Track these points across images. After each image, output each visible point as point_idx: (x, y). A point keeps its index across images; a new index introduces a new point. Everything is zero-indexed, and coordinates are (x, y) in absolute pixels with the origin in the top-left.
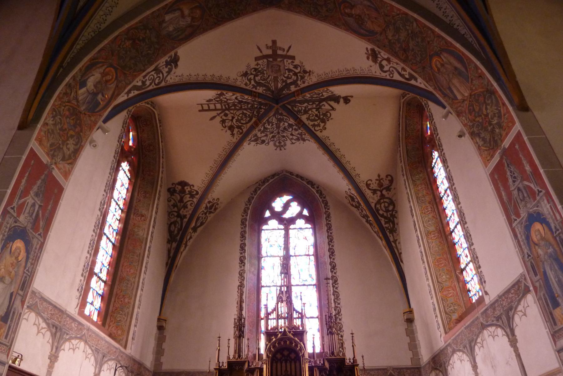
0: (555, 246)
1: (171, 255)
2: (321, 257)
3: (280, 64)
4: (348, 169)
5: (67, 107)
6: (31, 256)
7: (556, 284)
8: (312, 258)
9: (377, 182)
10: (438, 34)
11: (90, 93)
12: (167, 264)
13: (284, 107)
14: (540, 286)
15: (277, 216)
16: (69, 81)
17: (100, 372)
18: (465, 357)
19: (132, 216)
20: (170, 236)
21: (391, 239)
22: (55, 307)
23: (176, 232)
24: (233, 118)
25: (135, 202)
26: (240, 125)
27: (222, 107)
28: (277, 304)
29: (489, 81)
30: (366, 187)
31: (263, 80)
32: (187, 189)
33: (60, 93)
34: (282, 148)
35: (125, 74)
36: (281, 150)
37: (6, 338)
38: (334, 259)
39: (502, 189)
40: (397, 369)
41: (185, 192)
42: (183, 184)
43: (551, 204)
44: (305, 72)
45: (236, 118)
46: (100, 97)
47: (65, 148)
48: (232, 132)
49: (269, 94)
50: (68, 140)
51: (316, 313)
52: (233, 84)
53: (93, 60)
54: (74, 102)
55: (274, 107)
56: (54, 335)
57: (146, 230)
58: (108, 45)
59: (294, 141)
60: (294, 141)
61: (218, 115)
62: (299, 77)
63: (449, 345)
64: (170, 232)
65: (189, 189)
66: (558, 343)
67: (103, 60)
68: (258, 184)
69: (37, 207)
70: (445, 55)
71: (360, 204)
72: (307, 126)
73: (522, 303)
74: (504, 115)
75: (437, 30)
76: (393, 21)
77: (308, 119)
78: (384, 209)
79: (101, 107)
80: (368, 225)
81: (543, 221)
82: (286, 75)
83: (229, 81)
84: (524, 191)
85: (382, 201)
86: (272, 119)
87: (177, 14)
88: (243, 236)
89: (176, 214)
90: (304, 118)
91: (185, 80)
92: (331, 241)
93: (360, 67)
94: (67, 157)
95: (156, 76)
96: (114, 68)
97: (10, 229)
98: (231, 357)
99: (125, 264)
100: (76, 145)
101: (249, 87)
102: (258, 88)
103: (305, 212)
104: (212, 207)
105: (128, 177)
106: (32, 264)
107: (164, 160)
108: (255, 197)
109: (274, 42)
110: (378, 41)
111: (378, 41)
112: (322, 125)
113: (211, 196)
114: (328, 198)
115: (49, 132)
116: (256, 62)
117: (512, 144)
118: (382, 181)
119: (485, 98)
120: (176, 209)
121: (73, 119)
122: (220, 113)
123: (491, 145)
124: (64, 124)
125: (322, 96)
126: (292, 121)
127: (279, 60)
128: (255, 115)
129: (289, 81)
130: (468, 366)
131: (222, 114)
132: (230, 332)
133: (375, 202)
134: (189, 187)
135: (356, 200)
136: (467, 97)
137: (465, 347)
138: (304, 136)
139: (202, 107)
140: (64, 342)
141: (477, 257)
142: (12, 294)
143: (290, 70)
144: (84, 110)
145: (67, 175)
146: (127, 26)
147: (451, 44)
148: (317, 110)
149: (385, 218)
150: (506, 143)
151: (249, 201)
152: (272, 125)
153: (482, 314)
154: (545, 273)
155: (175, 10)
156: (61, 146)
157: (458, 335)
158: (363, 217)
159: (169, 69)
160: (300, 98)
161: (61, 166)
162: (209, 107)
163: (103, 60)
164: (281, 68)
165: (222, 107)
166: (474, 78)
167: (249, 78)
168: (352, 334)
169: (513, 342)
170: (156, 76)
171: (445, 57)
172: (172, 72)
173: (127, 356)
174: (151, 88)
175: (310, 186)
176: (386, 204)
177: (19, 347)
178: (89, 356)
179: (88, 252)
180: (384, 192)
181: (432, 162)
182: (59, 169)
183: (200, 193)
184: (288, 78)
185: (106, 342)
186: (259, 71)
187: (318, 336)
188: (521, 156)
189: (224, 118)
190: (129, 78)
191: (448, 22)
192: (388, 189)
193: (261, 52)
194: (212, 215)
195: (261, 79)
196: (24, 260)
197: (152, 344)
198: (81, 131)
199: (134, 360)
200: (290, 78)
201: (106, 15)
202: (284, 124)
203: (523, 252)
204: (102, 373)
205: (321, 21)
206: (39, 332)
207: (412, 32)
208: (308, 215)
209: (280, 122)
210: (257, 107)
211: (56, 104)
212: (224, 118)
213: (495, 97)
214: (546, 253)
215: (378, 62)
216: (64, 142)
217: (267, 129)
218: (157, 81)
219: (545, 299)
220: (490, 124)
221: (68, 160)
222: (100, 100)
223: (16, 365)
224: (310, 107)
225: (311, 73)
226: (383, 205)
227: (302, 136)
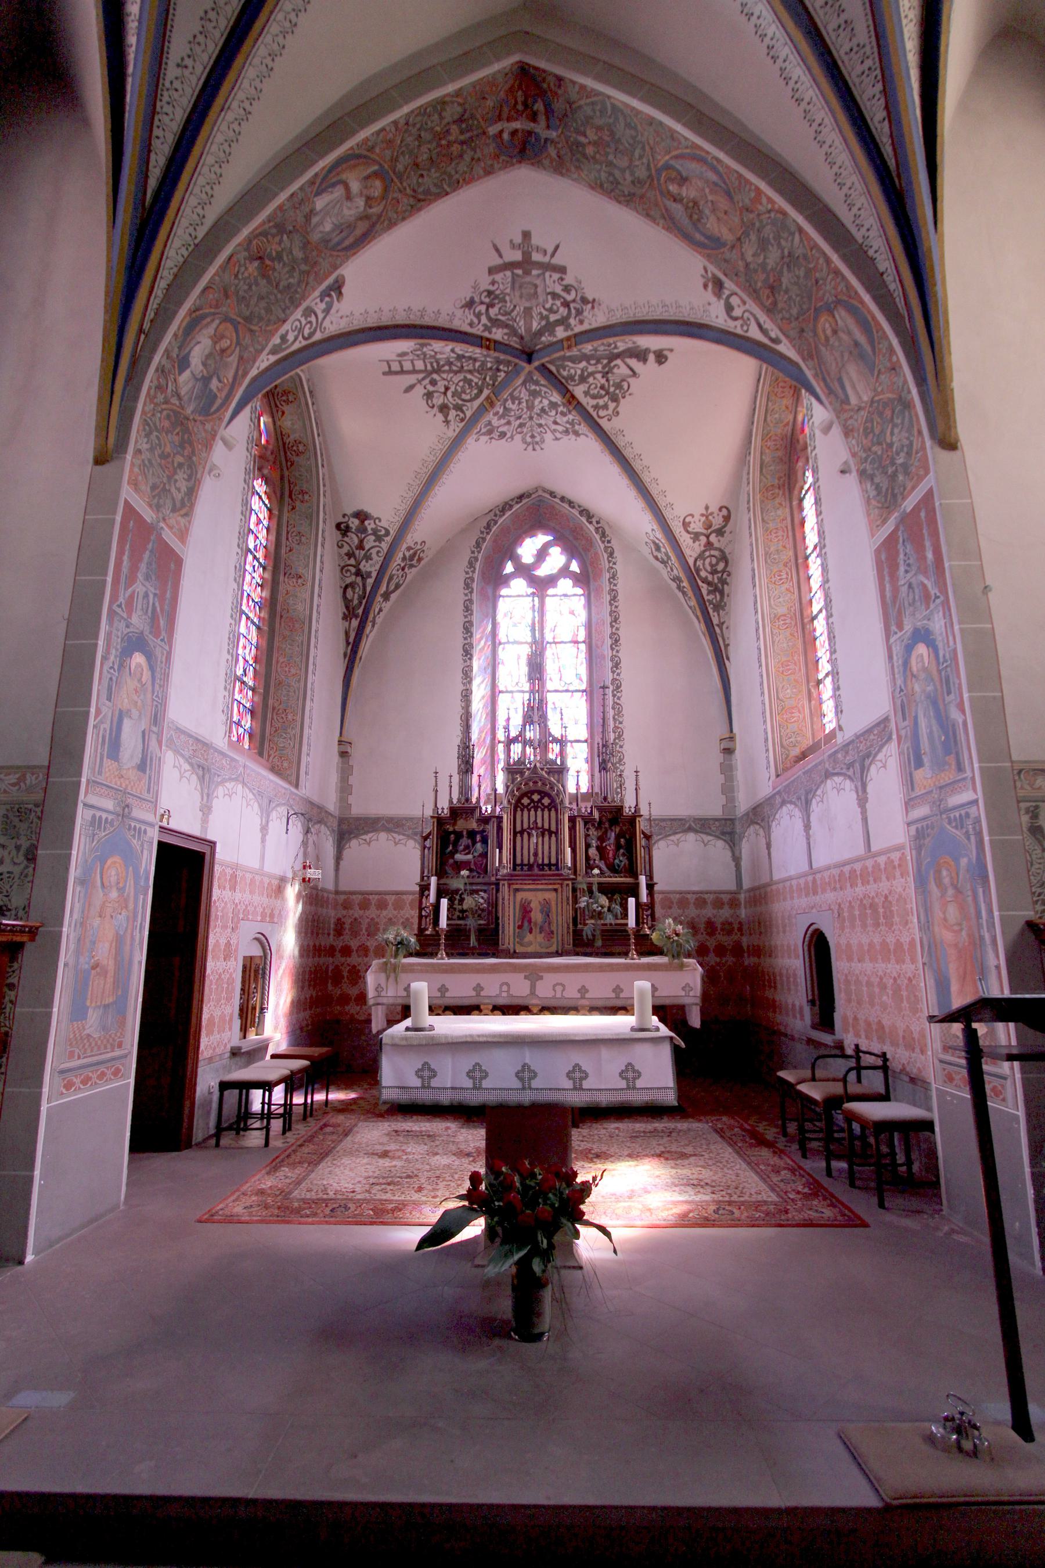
0: (938, 683)
1: (351, 640)
2: (597, 647)
3: (538, 282)
4: (654, 492)
5: (165, 413)
6: (158, 675)
7: (925, 736)
8: (583, 647)
9: (703, 519)
10: (836, 267)
11: (197, 380)
12: (345, 655)
13: (543, 369)
14: (906, 736)
15: (524, 571)
16: (160, 362)
17: (267, 822)
18: (797, 813)
19: (282, 578)
20: (347, 607)
21: (715, 621)
22: (197, 740)
23: (356, 602)
24: (447, 389)
25: (283, 551)
26: (460, 402)
27: (426, 366)
28: (524, 726)
29: (905, 382)
30: (682, 529)
31: (503, 315)
32: (369, 525)
33: (150, 388)
34: (537, 447)
35: (251, 331)
36: (534, 449)
37: (149, 791)
38: (618, 651)
39: (887, 578)
40: (701, 820)
41: (365, 530)
42: (362, 516)
43: (947, 620)
44: (584, 301)
45: (453, 389)
46: (214, 384)
47: (173, 490)
48: (446, 416)
49: (514, 342)
50: (175, 473)
51: (584, 734)
52: (447, 325)
53: (197, 310)
54: (175, 401)
55: (523, 368)
56: (202, 779)
57: (308, 601)
58: (217, 278)
59: (558, 435)
60: (558, 435)
61: (420, 382)
62: (573, 311)
63: (779, 793)
64: (347, 602)
65: (373, 526)
66: (910, 814)
67: (212, 310)
68: (492, 514)
69: (151, 596)
70: (843, 313)
71: (669, 558)
72: (585, 409)
73: (884, 750)
74: (917, 453)
75: (835, 257)
76: (757, 224)
77: (586, 393)
78: (709, 569)
79: (219, 402)
80: (680, 595)
81: (931, 644)
82: (548, 306)
83: (440, 320)
84: (917, 591)
85: (707, 554)
86: (520, 392)
87: (339, 192)
88: (468, 609)
89: (353, 570)
90: (579, 391)
91: (358, 323)
92: (615, 621)
93: (690, 303)
94: (178, 504)
95: (304, 322)
96: (231, 321)
97: (122, 639)
98: (455, 801)
99: (281, 660)
100: (189, 479)
101: (478, 330)
102: (494, 330)
103: (575, 567)
104: (414, 558)
105: (266, 505)
106: (160, 686)
107: (326, 469)
108: (488, 537)
109: (526, 235)
110: (726, 261)
111: (726, 261)
112: (612, 405)
113: (412, 538)
114: (614, 544)
115: (145, 465)
116: (491, 277)
117: (916, 509)
118: (710, 518)
119: (893, 412)
120: (352, 561)
121: (178, 434)
122: (423, 379)
123: (886, 500)
124: (165, 445)
125: (616, 347)
126: (556, 398)
127: (535, 272)
128: (488, 385)
129: (553, 318)
130: (799, 824)
131: (427, 381)
132: (451, 765)
133: (695, 555)
134: (372, 522)
135: (663, 550)
136: (866, 403)
137: (799, 798)
138: (577, 427)
139: (390, 367)
140: (216, 787)
141: (838, 673)
142: (144, 732)
143: (555, 296)
144: (192, 412)
145: (183, 535)
146: (245, 232)
147: (856, 293)
148: (605, 375)
149: (709, 584)
150: (909, 504)
151: (478, 545)
152: (520, 403)
153: (830, 756)
154: (916, 718)
155: (334, 185)
156: (167, 487)
157: (793, 781)
158: (673, 580)
159: (327, 303)
160: (574, 352)
161: (172, 522)
162: (402, 367)
163: (212, 310)
164: (539, 290)
165: (426, 366)
166: (883, 370)
167: (477, 311)
168: (636, 772)
169: (862, 801)
170: (304, 322)
171: (841, 318)
172: (333, 311)
173: (302, 798)
174: (296, 346)
175: (584, 520)
176: (714, 560)
177: (165, 802)
178: (251, 803)
179: (229, 652)
180: (713, 538)
181: (802, 488)
182: (171, 528)
183: (392, 532)
184: (551, 310)
185: (271, 781)
186: (496, 297)
187: (585, 767)
188: (924, 531)
189: (431, 388)
190: (260, 339)
191: (860, 241)
192: (720, 532)
193: (501, 256)
194: (414, 570)
195: (500, 313)
196: (150, 683)
197: (334, 778)
198: (193, 452)
199: (311, 803)
200: (556, 312)
201: (203, 205)
202: (541, 402)
203: (895, 684)
204: (270, 823)
205: (620, 202)
206: (181, 777)
207: (790, 254)
208: (578, 571)
209: (535, 398)
210: (491, 368)
211: (147, 409)
212: (431, 388)
213: (910, 414)
214: (924, 691)
215: (724, 297)
216: (169, 478)
217: (510, 410)
218: (306, 332)
219: (909, 755)
220: (893, 463)
221: (180, 509)
222: (215, 390)
223: (164, 824)
224: (591, 369)
225: (596, 305)
226: (708, 561)
227: (573, 426)
